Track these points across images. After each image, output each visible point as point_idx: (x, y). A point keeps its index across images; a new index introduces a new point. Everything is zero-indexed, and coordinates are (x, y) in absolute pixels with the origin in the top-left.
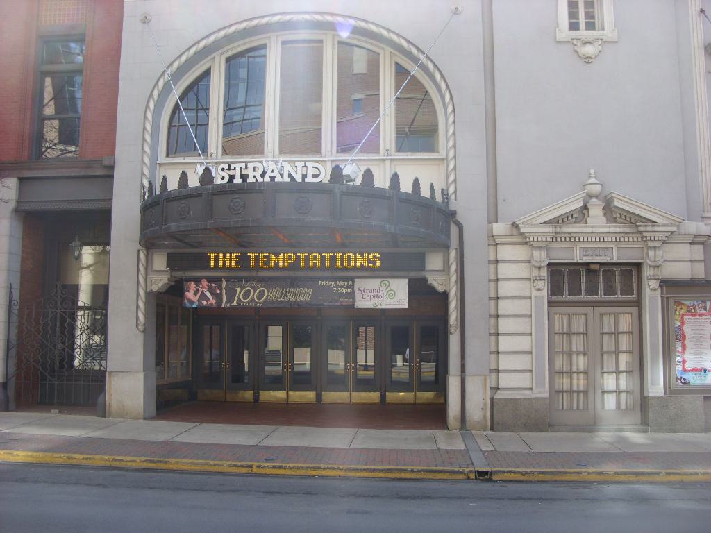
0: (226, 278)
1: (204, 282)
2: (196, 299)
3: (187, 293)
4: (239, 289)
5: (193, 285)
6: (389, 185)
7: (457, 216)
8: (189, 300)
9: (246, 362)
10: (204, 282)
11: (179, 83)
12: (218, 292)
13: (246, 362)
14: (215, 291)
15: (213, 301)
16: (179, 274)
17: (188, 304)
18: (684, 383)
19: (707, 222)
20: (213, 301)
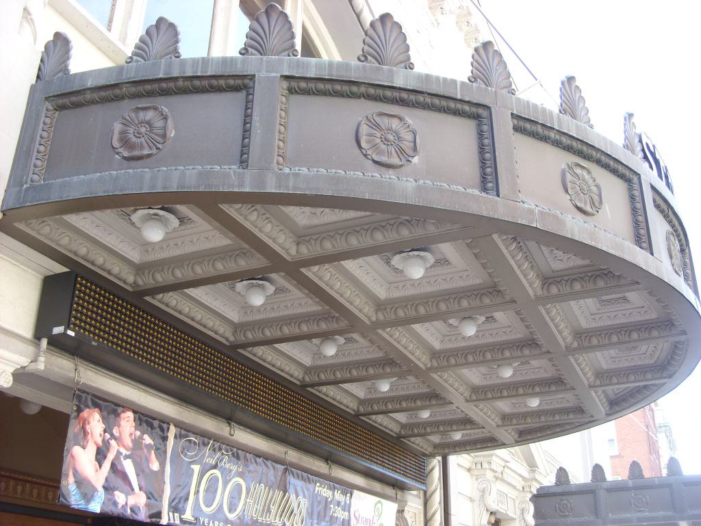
0: (179, 425)
1: (127, 421)
2: (97, 476)
3: (77, 450)
4: (196, 468)
5: (95, 423)
6: (591, 479)
7: (136, 44)
8: (81, 482)
9: (645, 524)
10: (127, 421)
11: (314, 52)
12: (155, 466)
13: (645, 524)
14: (148, 460)
15: (139, 499)
16: (63, 367)
17: (75, 499)
18: (627, 348)
19: (604, 298)
20: (139, 499)
